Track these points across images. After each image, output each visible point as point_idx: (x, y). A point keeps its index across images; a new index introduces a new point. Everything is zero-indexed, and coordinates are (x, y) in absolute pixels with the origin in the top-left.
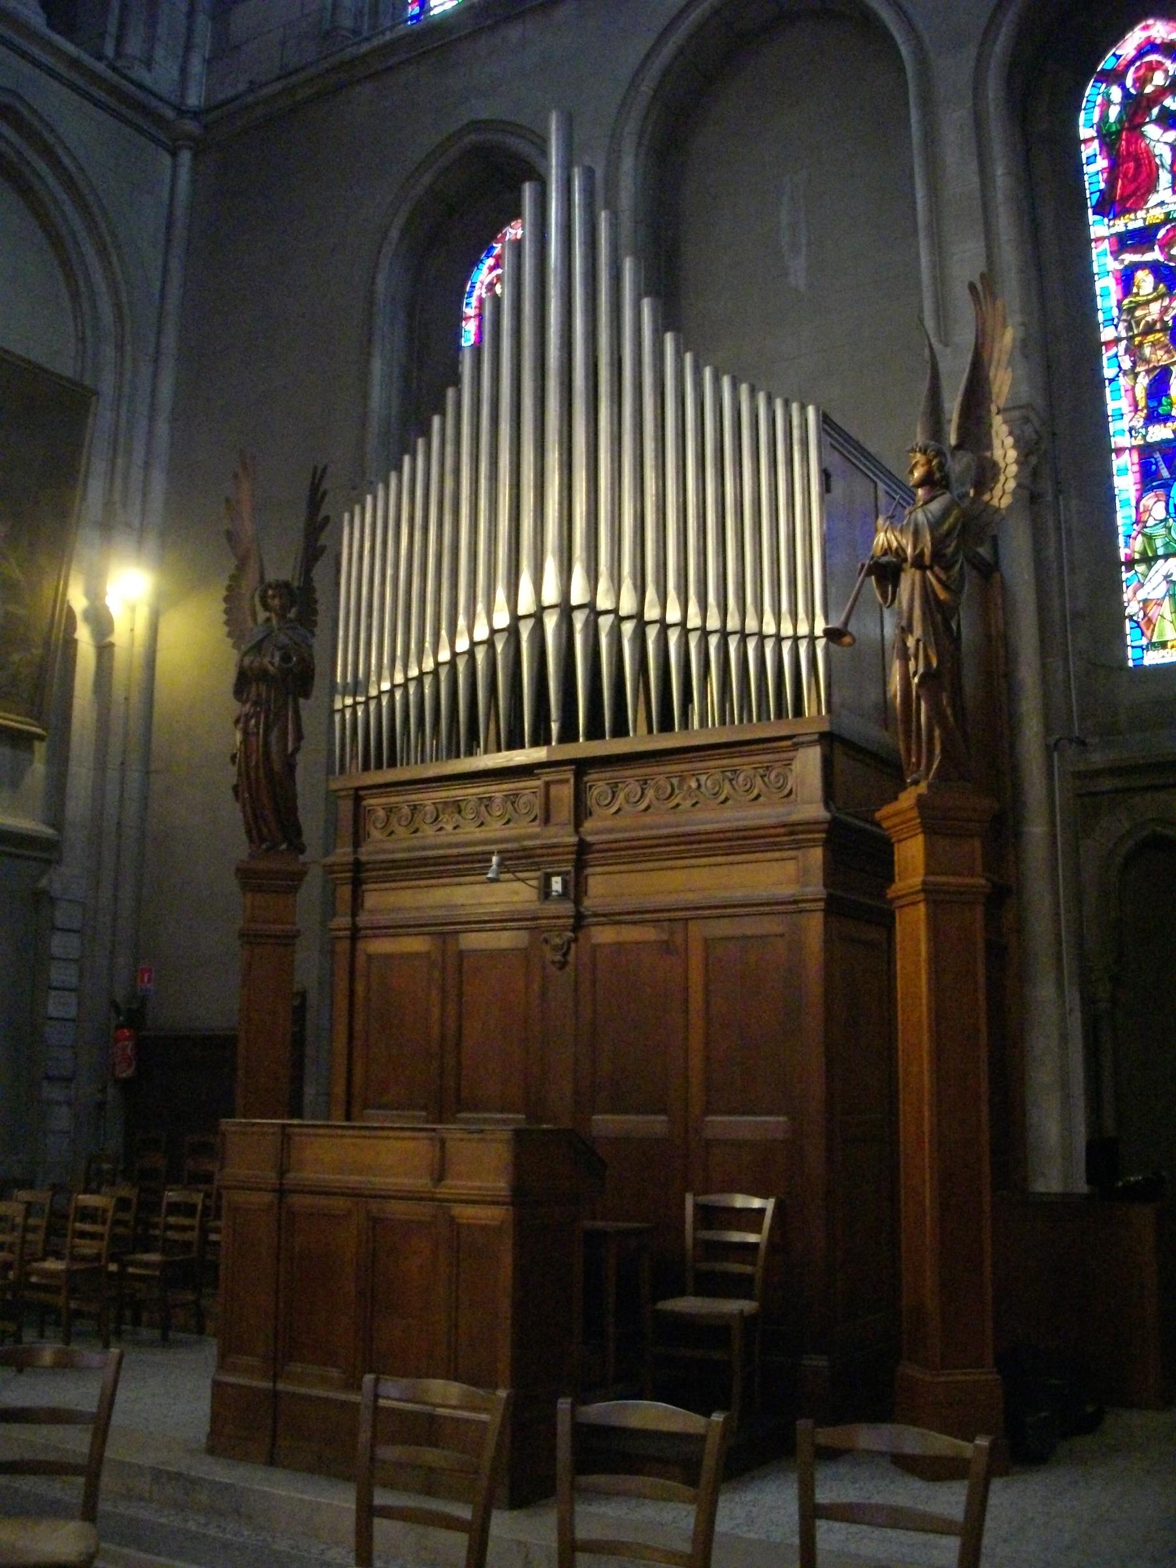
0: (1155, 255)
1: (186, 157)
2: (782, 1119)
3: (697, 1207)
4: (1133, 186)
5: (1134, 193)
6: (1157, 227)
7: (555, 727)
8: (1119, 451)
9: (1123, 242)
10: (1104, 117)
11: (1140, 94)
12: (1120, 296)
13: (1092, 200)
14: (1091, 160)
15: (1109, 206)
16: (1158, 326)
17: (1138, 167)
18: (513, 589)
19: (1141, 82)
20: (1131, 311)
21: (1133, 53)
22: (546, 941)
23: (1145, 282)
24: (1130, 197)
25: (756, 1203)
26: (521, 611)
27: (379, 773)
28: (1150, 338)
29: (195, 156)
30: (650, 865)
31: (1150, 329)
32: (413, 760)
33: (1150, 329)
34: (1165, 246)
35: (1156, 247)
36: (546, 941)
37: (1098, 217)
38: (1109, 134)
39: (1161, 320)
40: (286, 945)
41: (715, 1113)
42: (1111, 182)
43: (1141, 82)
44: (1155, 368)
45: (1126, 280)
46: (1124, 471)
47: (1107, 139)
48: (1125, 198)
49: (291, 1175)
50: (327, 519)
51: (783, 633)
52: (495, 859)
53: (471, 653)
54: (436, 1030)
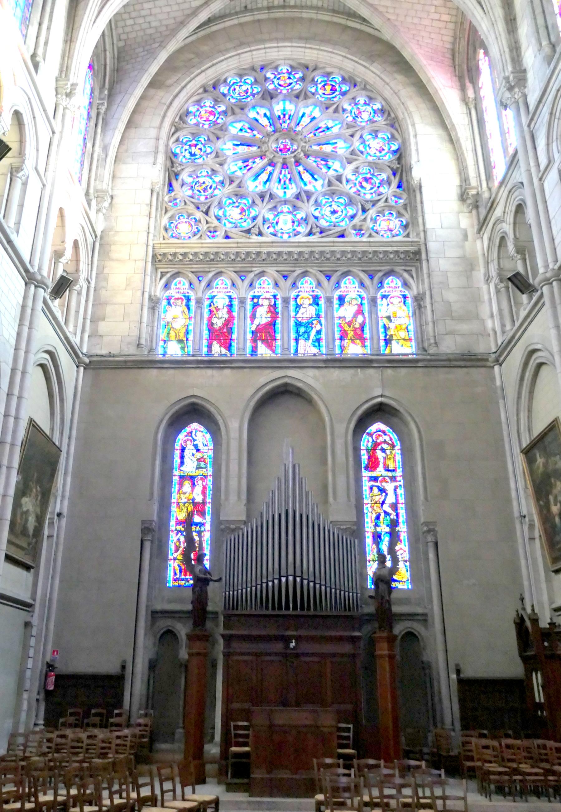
0: (378, 484)
1: (82, 369)
7: (291, 606)
8: (368, 532)
10: (367, 445)
17: (375, 460)
18: (403, 618)
19: (377, 438)
23: (375, 490)
26: (282, 574)
29: (85, 369)
32: (13, 548)
33: (376, 503)
34: (381, 482)
42: (369, 462)
43: (377, 438)
45: (371, 488)
46: (368, 537)
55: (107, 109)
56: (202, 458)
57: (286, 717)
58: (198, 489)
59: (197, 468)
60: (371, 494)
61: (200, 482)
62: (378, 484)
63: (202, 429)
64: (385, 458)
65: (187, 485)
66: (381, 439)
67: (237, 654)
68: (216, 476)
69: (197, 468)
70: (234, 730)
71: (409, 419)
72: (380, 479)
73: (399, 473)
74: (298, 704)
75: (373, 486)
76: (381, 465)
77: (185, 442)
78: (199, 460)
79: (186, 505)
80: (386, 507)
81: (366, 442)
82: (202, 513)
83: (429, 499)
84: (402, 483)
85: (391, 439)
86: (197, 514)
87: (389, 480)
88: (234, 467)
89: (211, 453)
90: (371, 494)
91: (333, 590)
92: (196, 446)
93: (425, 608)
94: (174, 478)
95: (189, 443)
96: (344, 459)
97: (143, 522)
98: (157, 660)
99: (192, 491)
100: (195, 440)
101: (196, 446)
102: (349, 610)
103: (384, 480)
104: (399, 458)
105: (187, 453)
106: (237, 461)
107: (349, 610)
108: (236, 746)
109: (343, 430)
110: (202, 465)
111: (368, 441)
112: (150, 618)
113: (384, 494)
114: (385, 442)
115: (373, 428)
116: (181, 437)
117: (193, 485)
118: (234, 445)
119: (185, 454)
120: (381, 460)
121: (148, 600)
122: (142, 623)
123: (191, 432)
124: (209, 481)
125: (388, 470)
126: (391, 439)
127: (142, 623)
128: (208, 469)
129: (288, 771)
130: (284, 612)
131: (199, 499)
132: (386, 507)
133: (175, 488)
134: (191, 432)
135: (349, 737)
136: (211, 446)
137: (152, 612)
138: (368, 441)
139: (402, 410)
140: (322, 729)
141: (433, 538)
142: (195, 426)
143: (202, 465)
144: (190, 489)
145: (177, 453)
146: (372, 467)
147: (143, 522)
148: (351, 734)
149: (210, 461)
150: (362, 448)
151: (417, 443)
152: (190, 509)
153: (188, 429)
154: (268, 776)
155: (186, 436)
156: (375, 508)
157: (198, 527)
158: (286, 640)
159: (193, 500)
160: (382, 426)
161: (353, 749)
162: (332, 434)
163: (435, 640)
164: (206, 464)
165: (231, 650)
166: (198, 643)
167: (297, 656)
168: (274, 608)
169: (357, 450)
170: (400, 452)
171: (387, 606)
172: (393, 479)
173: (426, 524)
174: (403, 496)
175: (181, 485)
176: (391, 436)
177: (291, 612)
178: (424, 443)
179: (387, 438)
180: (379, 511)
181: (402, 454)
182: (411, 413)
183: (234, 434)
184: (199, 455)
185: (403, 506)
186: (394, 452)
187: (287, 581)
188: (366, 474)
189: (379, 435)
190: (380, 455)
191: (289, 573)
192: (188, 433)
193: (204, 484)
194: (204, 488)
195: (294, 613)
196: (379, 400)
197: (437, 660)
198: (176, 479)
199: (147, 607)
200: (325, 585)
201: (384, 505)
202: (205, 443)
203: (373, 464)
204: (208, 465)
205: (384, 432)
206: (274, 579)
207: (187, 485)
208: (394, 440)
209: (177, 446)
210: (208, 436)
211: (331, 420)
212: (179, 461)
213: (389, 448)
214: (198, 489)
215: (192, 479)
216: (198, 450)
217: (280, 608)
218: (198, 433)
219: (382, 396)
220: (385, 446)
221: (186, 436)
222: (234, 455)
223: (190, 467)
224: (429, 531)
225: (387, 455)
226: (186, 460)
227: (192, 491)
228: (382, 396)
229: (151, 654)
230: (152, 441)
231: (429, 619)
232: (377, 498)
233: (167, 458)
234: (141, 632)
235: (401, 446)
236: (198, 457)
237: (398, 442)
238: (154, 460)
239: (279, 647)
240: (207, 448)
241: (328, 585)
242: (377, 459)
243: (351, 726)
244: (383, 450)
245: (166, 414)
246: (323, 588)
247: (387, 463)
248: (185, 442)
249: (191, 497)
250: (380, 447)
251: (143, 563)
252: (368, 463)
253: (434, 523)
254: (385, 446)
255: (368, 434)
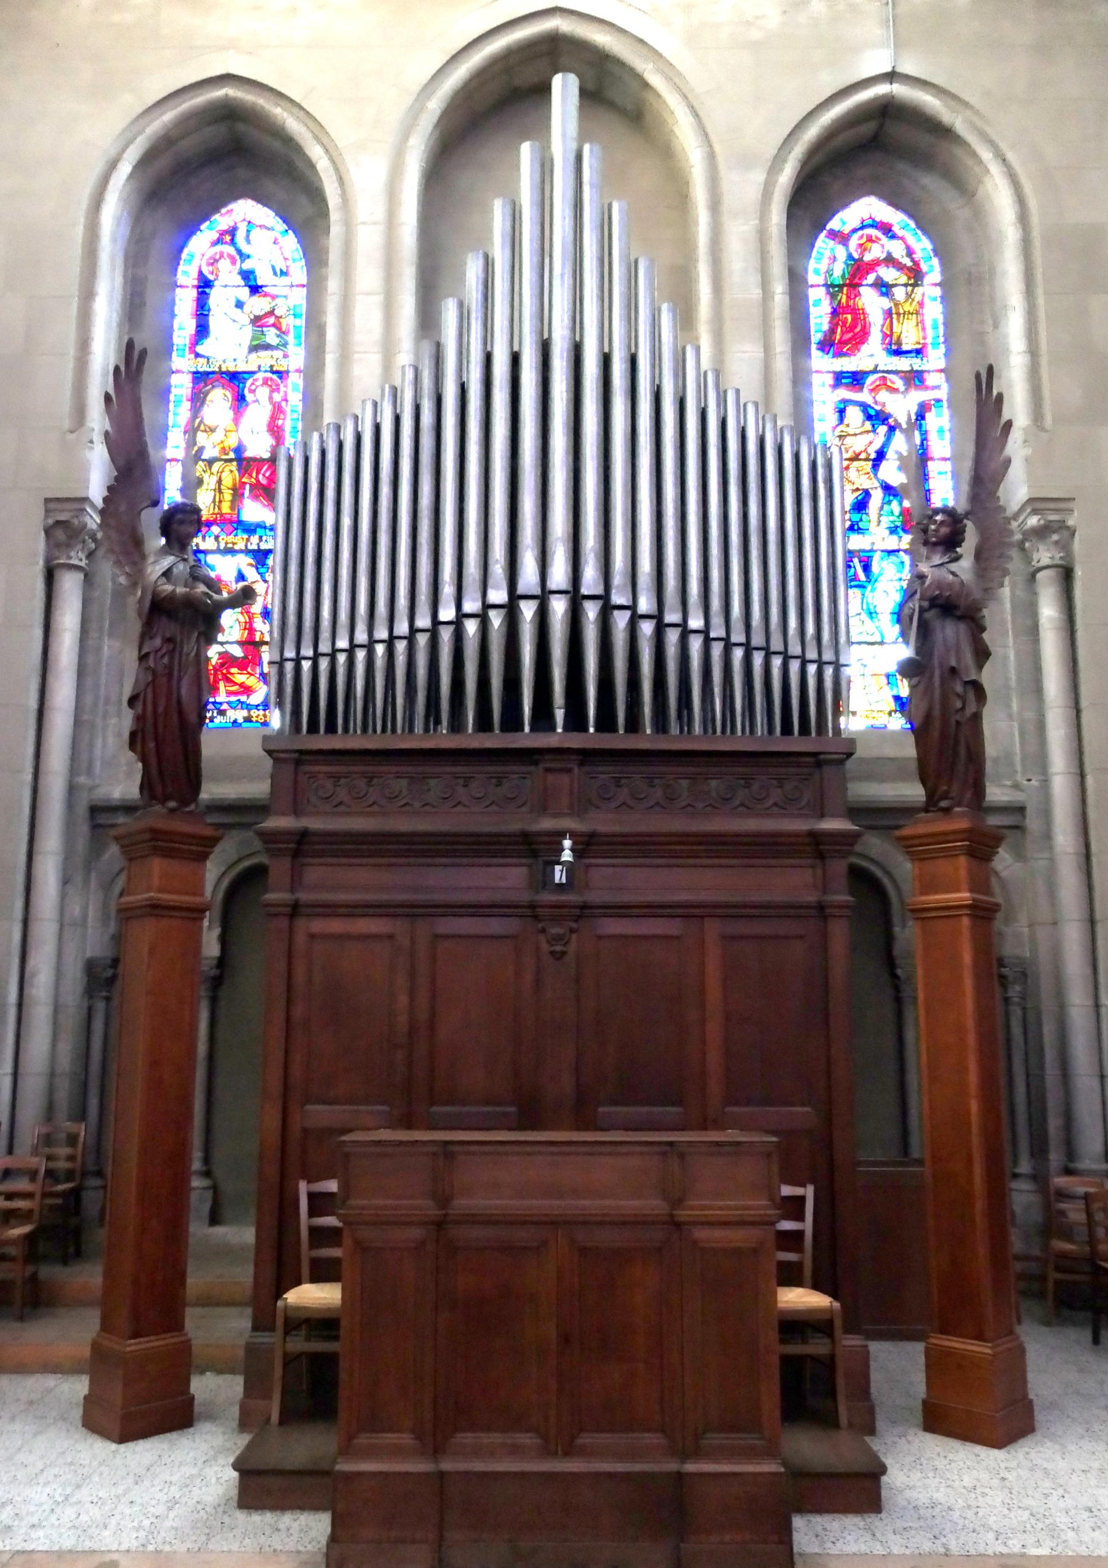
0: (864, 396)
2: (807, 1109)
3: (311, 1196)
4: (850, 335)
7: (560, 715)
9: (839, 378)
10: (829, 272)
13: (816, 337)
14: (817, 303)
23: (854, 415)
25: (798, 1191)
26: (521, 589)
28: (856, 464)
30: (660, 861)
33: (856, 458)
38: (833, 286)
40: (194, 919)
41: (737, 1103)
44: (858, 489)
47: (831, 289)
48: (843, 342)
53: (483, 618)
54: (403, 1019)
55: (315, 287)
56: (271, 313)
57: (517, 1177)
58: (258, 412)
59: (254, 349)
61: (263, 393)
62: (864, 396)
64: (888, 314)
65: (219, 399)
66: (875, 253)
70: (313, 1212)
71: (986, 155)
73: (935, 359)
75: (845, 401)
77: (214, 262)
78: (257, 321)
79: (216, 466)
82: (265, 492)
83: (1048, 421)
84: (943, 394)
85: (910, 252)
86: (254, 497)
87: (899, 384)
91: (738, 654)
92: (247, 276)
94: (174, 379)
95: (224, 265)
96: (756, 293)
98: (115, 962)
99: (236, 421)
100: (243, 256)
101: (247, 276)
102: (805, 730)
104: (934, 311)
105: (217, 298)
106: (379, 299)
107: (805, 730)
108: (315, 1279)
112: (84, 829)
113: (882, 430)
114: (890, 261)
115: (846, 218)
117: (239, 400)
118: (368, 241)
122: (51, 841)
125: (898, 353)
126: (910, 252)
127: (51, 841)
128: (291, 349)
130: (527, 738)
131: (259, 446)
133: (179, 413)
134: (232, 232)
135: (799, 1235)
138: (834, 259)
142: (244, 211)
145: (185, 301)
146: (843, 342)
147: (49, 501)
148: (808, 1225)
149: (295, 324)
150: (812, 279)
153: (221, 221)
157: (255, 539)
159: (239, 450)
162: (715, 206)
167: (585, 911)
168: (484, 723)
169: (796, 280)
170: (938, 291)
171: (971, 708)
172: (915, 378)
174: (947, 436)
175: (197, 400)
176: (911, 241)
178: (1036, 233)
179: (897, 250)
180: (865, 483)
184: (258, 305)
185: (948, 466)
187: (543, 614)
188: (823, 364)
189: (870, 239)
190: (871, 302)
192: (222, 233)
193: (277, 397)
194: (278, 410)
195: (575, 741)
196: (882, 89)
198: (181, 385)
199: (72, 789)
201: (884, 465)
202: (281, 265)
203: (847, 332)
204: (290, 338)
205: (886, 229)
206: (487, 606)
207: (219, 399)
209: (187, 274)
210: (290, 241)
211: (711, 157)
212: (191, 326)
213: (904, 279)
214: (258, 412)
215: (234, 379)
217: (512, 721)
218: (255, 233)
219: (891, 76)
220: (888, 274)
223: (227, 346)
225: (897, 305)
226: (214, 322)
227: (236, 421)
229: (95, 942)
230: (79, 231)
231: (1032, 823)
232: (857, 444)
235: (943, 271)
237: (935, 261)
239: (509, 879)
240: (285, 280)
242: (858, 314)
243: (809, 1192)
244: (884, 288)
247: (897, 328)
248: (214, 262)
249: (232, 442)
250: (871, 278)
252: (832, 330)
253: (1062, 503)
254: (888, 274)
255: (833, 235)
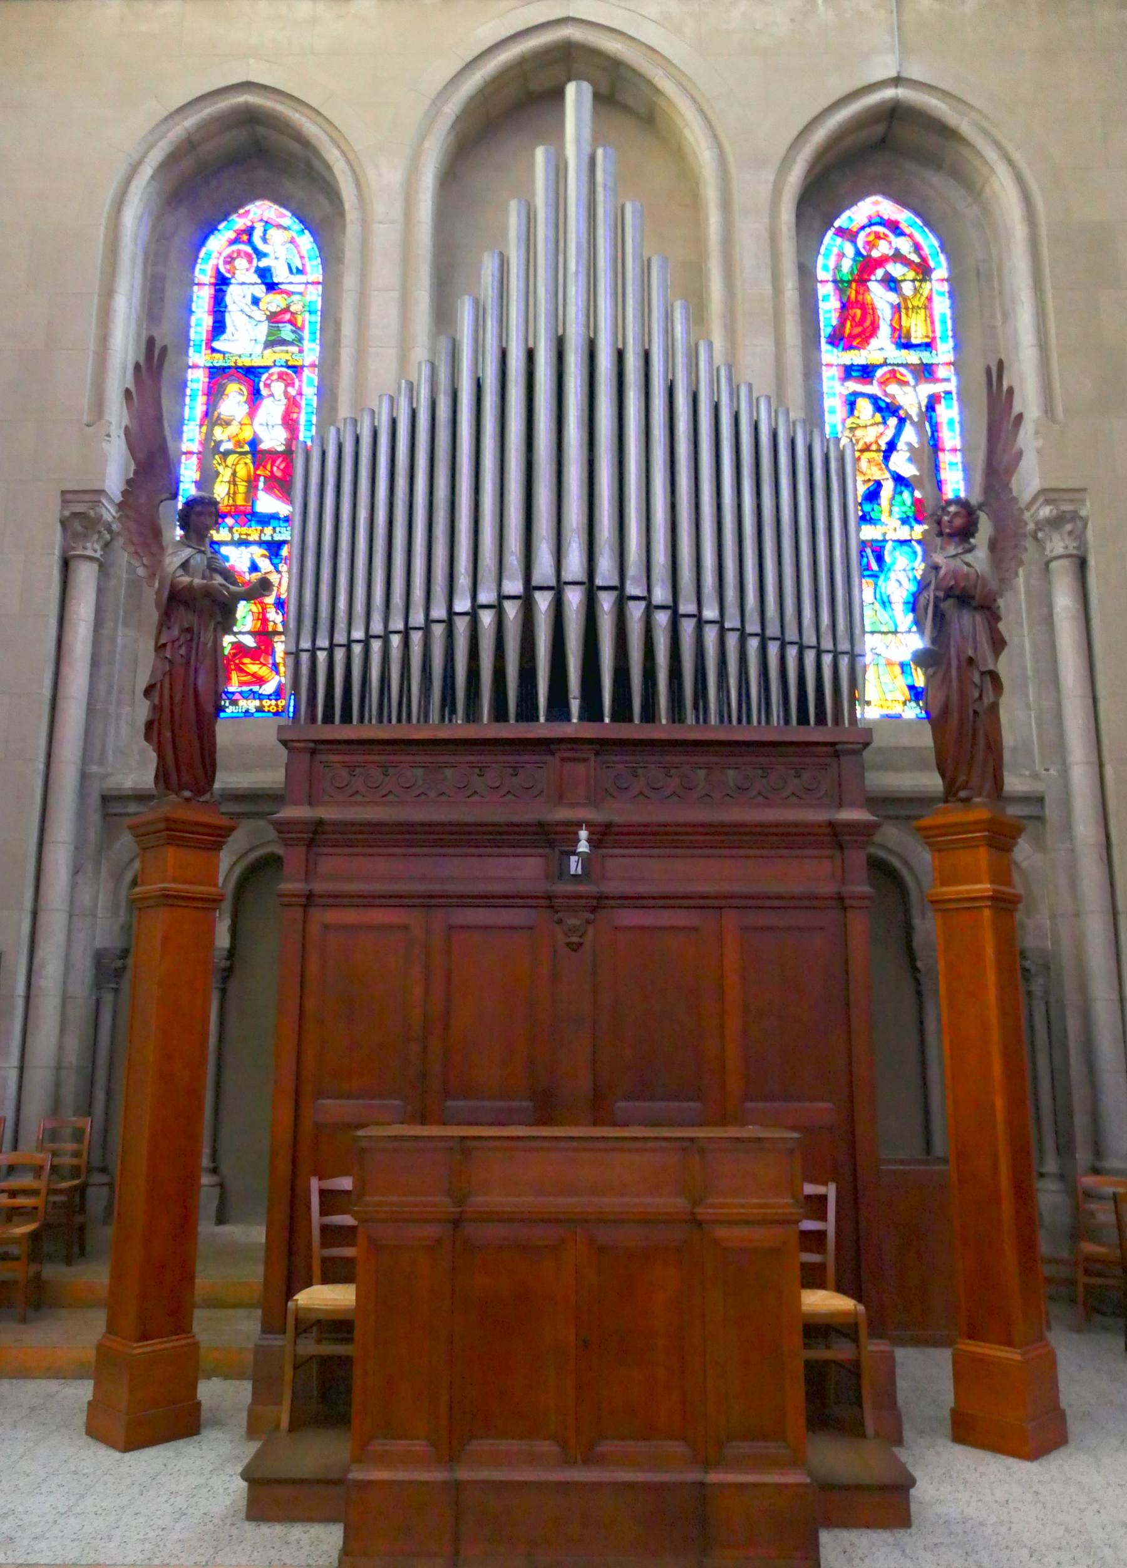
0: (873, 389)
5: (859, 335)
6: (876, 367)
7: (575, 705)
9: (848, 372)
10: (838, 267)
11: (869, 256)
12: (844, 415)
13: (825, 331)
14: (826, 298)
15: (837, 339)
16: (874, 447)
20: (852, 429)
21: (864, 221)
22: (560, 922)
23: (864, 407)
24: (855, 337)
25: (820, 1190)
27: (329, 727)
31: (867, 449)
33: (867, 449)
34: (883, 383)
35: (875, 382)
36: (560, 922)
37: (829, 347)
38: (842, 281)
39: (876, 442)
44: (869, 480)
48: (852, 337)
49: (478, 1199)
50: (1011, 391)
51: (806, 642)
52: (583, 834)
53: (473, 616)
56: (286, 310)
58: (272, 409)
59: (270, 344)
60: (849, 422)
61: (278, 388)
62: (873, 389)
63: (288, 220)
64: (897, 309)
66: (882, 249)
67: (338, 900)
68: (328, 366)
69: (270, 344)
71: (992, 155)
72: (879, 373)
73: (944, 352)
74: (599, 1110)
75: (856, 394)
76: (884, 331)
77: (230, 260)
78: (274, 318)
79: (231, 459)
80: (901, 462)
81: (834, 257)
84: (952, 386)
85: (917, 248)
87: (909, 377)
88: (384, 313)
89: (315, 295)
90: (849, 422)
92: (264, 274)
93: (1035, 776)
94: (191, 374)
95: (241, 263)
96: (768, 289)
97: (66, 496)
98: (125, 953)
99: (252, 414)
100: (260, 255)
101: (264, 274)
102: (821, 719)
103: (893, 377)
104: (942, 306)
105: (234, 296)
107: (821, 719)
108: (326, 1280)
109: (764, 192)
110: (286, 332)
111: (841, 255)
112: (95, 817)
113: (893, 421)
114: (898, 257)
116: (217, 244)
117: (255, 397)
119: (228, 299)
120: (884, 313)
121: (86, 758)
123: (249, 231)
124: (308, 386)
125: (908, 346)
126: (917, 248)
128: (306, 345)
129: (546, 1447)
130: (542, 727)
131: (274, 439)
132: (901, 462)
133: (195, 407)
134: (249, 231)
135: (821, 1235)
136: (315, 272)
137: (105, 799)
139: (965, 128)
140: (722, 1232)
141: (1072, 544)
142: (260, 210)
143: (286, 332)
144: (245, 408)
145: (202, 298)
147: (66, 496)
149: (311, 322)
150: (821, 275)
151: (1019, 231)
152: (242, 472)
153: (238, 222)
154: (438, 1475)
155: (232, 242)
156: (863, 464)
158: (553, 839)
159: (254, 443)
160: (888, 208)
161: (840, 1289)
162: (726, 205)
163: (1074, 882)
164: (298, 330)
165: (318, 887)
166: (171, 854)
167: (598, 904)
170: (945, 287)
172: (926, 372)
173: (1048, 494)
174: (957, 427)
175: (214, 392)
176: (919, 237)
177: (575, 726)
178: (1043, 232)
179: (904, 246)
180: (876, 474)
181: (952, 295)
182: (1000, 137)
183: (385, 209)
184: (274, 302)
185: (958, 458)
186: (926, 287)
187: (558, 605)
188: (832, 357)
189: (878, 237)
190: (880, 297)
191: (567, 576)
192: (240, 233)
193: (292, 391)
194: (293, 404)
195: (590, 731)
196: (889, 93)
197: (1079, 943)
200: (720, 622)
201: (894, 456)
202: (297, 263)
203: (856, 326)
204: (306, 334)
205: (894, 227)
206: (502, 597)
208: (927, 251)
209: (204, 273)
210: (306, 241)
212: (208, 321)
213: (911, 275)
214: (272, 409)
215: (250, 374)
216: (271, 287)
217: (527, 711)
218: (273, 233)
219: (897, 81)
220: (896, 270)
221: (232, 242)
222: (385, 274)
223: (244, 340)
224: (1055, 523)
225: (906, 299)
227: (252, 414)
228: (897, 81)
229: (104, 933)
231: (1052, 812)
232: (868, 435)
233: (161, 298)
234: (60, 859)
236: (274, 309)
237: (942, 257)
238: (108, 293)
239: (525, 870)
241: (732, 622)
242: (868, 310)
243: (831, 1191)
244: (891, 283)
245: (152, 146)
246: (711, 635)
248: (230, 260)
249: (247, 435)
250: (879, 273)
251: (68, 637)
